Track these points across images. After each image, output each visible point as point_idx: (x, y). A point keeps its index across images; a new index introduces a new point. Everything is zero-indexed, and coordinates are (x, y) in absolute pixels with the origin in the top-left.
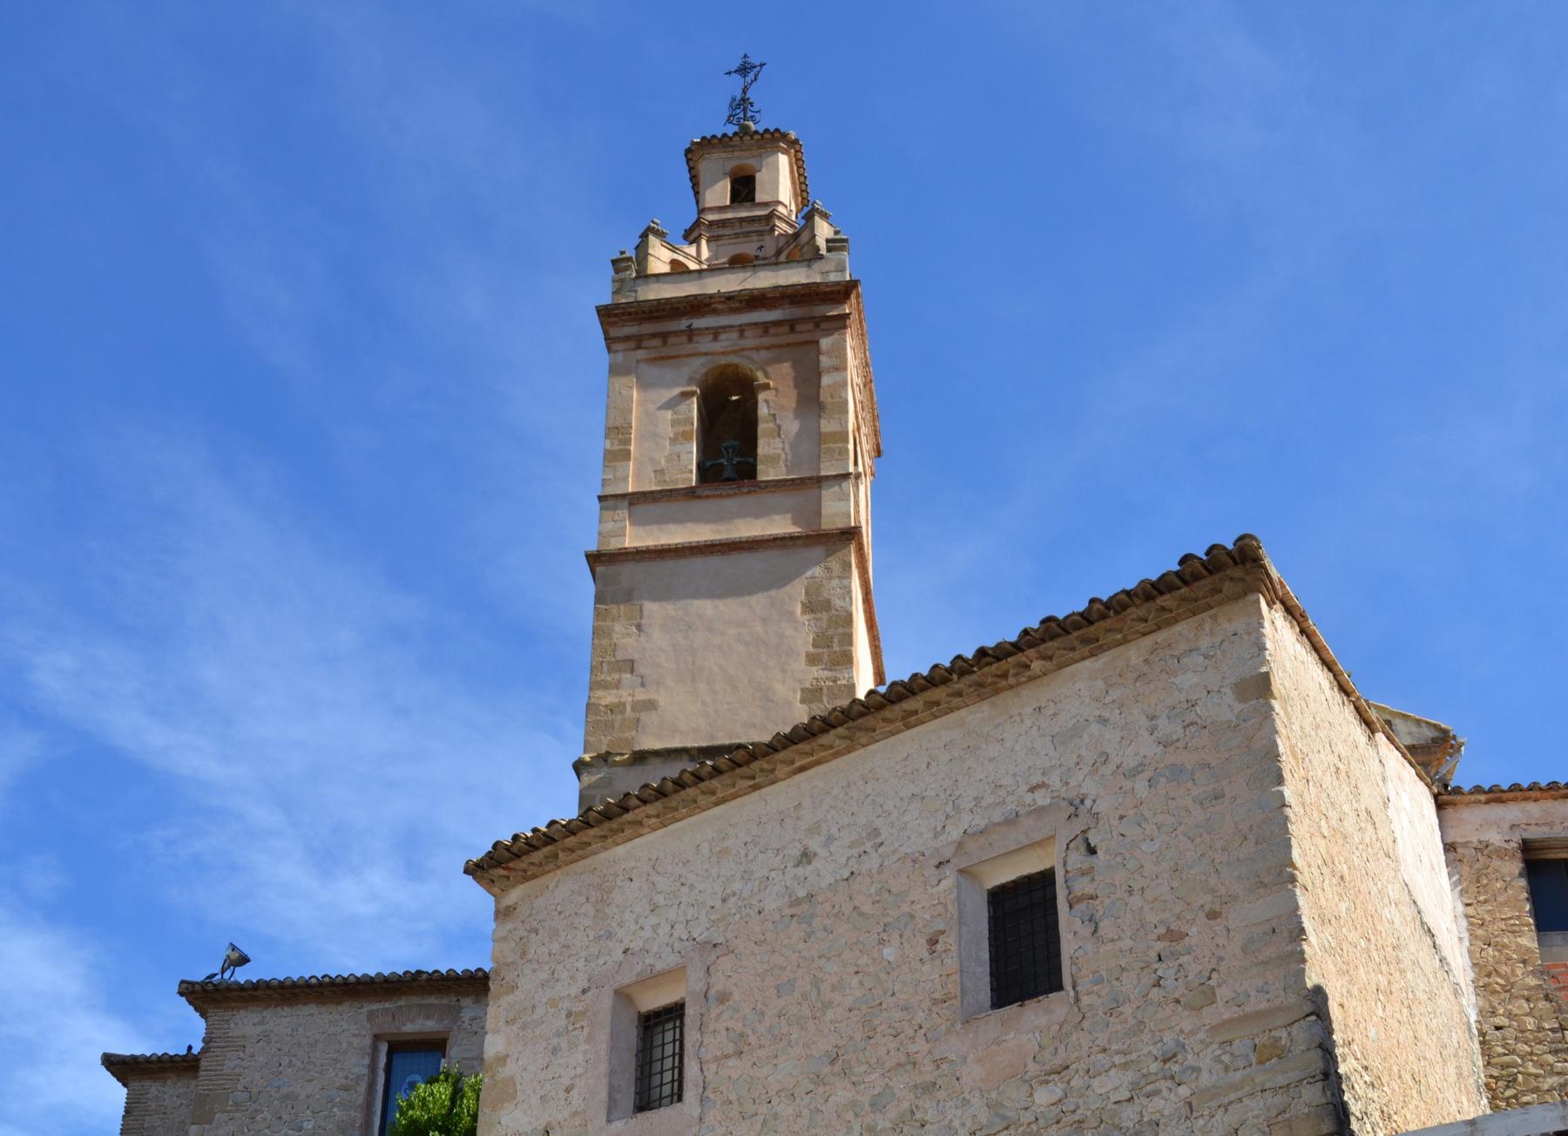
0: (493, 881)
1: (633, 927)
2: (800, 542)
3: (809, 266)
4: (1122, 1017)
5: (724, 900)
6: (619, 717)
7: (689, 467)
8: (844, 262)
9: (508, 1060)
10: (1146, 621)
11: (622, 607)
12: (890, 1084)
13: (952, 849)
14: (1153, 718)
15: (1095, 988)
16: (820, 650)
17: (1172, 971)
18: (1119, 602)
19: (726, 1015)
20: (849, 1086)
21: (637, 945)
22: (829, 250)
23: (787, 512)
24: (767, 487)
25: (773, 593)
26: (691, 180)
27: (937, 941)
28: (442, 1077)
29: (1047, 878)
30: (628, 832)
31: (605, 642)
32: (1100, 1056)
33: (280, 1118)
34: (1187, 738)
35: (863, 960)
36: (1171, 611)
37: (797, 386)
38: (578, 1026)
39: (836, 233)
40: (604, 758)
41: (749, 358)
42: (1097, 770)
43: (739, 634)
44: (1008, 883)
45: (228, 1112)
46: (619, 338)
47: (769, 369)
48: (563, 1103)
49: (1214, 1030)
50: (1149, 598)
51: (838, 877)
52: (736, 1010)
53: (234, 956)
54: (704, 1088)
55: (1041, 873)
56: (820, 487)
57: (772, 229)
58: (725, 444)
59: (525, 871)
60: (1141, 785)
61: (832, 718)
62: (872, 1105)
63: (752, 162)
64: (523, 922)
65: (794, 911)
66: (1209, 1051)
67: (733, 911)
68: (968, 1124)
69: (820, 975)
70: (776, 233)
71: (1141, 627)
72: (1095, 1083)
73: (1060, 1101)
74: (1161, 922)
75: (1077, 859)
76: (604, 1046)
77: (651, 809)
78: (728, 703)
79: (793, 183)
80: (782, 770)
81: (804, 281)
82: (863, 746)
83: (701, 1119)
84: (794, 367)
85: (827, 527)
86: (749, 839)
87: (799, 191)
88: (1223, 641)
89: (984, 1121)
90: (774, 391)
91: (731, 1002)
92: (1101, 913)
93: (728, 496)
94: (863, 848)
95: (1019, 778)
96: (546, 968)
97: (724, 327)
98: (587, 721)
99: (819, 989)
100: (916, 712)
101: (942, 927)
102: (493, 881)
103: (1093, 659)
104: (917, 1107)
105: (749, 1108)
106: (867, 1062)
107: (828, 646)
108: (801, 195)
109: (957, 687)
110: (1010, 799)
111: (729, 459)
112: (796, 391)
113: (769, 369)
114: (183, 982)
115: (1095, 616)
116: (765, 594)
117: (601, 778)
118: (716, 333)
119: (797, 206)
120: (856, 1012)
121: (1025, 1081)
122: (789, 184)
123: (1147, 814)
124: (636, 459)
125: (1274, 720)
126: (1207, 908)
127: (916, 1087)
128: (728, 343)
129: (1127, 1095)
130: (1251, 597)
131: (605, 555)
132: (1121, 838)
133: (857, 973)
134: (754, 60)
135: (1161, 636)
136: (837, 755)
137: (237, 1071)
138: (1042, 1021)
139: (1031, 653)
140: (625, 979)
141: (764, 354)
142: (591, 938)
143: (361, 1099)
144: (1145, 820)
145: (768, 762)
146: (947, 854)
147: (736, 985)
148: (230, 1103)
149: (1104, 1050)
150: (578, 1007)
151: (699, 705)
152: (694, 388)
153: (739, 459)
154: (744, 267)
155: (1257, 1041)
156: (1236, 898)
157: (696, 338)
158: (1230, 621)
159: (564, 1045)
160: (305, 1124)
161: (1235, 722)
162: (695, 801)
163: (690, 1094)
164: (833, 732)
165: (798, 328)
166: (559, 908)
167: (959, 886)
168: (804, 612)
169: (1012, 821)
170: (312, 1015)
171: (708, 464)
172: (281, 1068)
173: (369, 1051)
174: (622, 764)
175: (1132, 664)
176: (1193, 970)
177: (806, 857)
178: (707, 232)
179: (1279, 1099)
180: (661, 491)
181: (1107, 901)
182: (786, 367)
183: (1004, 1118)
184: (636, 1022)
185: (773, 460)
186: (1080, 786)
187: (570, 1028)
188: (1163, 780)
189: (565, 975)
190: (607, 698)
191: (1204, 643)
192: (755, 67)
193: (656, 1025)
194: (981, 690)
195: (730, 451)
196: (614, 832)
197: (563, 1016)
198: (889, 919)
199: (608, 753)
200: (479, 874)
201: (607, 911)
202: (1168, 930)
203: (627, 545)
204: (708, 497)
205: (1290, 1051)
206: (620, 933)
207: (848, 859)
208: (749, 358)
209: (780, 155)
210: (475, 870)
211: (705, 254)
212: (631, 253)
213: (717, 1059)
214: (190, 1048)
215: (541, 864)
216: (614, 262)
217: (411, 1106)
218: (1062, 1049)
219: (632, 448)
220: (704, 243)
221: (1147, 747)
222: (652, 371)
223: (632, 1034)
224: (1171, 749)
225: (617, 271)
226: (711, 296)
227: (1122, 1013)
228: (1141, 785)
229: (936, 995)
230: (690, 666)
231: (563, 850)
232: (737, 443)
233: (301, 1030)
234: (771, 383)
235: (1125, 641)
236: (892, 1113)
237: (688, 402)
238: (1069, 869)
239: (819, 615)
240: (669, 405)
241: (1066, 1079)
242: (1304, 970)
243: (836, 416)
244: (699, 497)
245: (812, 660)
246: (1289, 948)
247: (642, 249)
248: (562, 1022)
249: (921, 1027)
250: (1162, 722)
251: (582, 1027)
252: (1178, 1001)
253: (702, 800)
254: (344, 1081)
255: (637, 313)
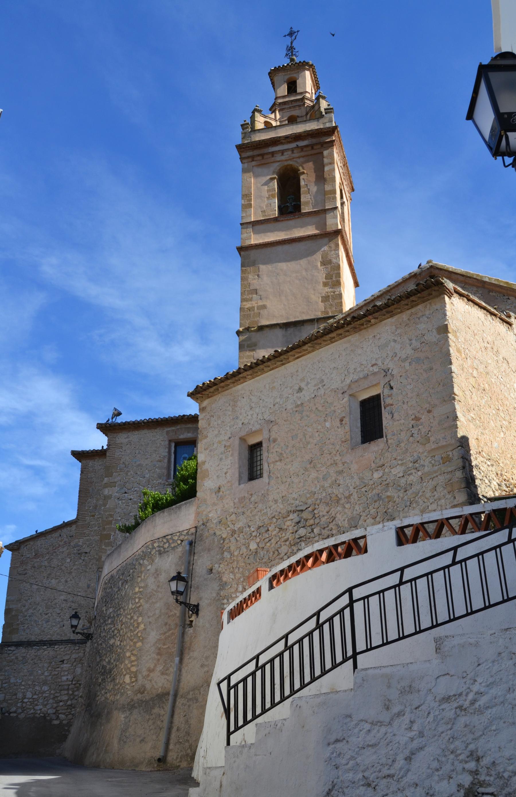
0: (197, 398)
1: (245, 415)
2: (319, 237)
3: (318, 121)
4: (401, 447)
5: (274, 405)
6: (253, 312)
7: (275, 209)
8: (332, 118)
9: (206, 463)
10: (408, 305)
11: (251, 268)
12: (329, 471)
13: (347, 387)
14: (411, 340)
15: (393, 437)
16: (328, 280)
17: (417, 431)
18: (397, 299)
19: (276, 446)
20: (316, 472)
21: (246, 421)
22: (326, 114)
23: (313, 225)
24: (305, 215)
25: (309, 258)
26: (272, 84)
27: (343, 420)
28: (193, 457)
29: (378, 397)
30: (242, 380)
31: (245, 282)
32: (394, 461)
33: (137, 473)
34: (422, 348)
35: (320, 427)
36: (416, 301)
37: (315, 172)
38: (228, 450)
39: (329, 105)
40: (247, 329)
41: (296, 161)
42: (393, 359)
43: (297, 276)
44: (366, 399)
45: (118, 472)
46: (245, 157)
47: (304, 166)
48: (224, 478)
49: (429, 452)
50: (408, 298)
51: (311, 397)
52: (279, 445)
53: (116, 412)
54: (270, 473)
55: (377, 395)
56: (326, 213)
57: (304, 104)
58: (289, 197)
59: (208, 395)
60: (407, 364)
61: (306, 341)
62: (323, 478)
63: (295, 75)
64: (209, 413)
65: (297, 409)
66: (428, 459)
67: (277, 409)
68: (353, 485)
69: (306, 432)
70: (306, 105)
71: (406, 307)
72: (392, 470)
73: (381, 477)
74: (413, 414)
75: (387, 391)
76: (237, 458)
77: (248, 373)
78: (293, 304)
79: (313, 81)
80: (291, 358)
81: (316, 128)
82: (318, 349)
83: (269, 483)
84: (314, 164)
85: (329, 230)
86: (281, 383)
87: (315, 84)
88: (433, 312)
89: (358, 484)
90: (306, 175)
91: (277, 442)
92: (394, 410)
93: (291, 219)
94: (319, 387)
95: (368, 362)
96: (217, 429)
97: (286, 150)
98: (240, 315)
99: (305, 437)
100: (334, 338)
101: (344, 415)
102: (197, 398)
103: (392, 318)
104: (337, 479)
105: (284, 480)
106: (321, 463)
107: (331, 279)
108: (316, 85)
109: (347, 329)
110: (365, 369)
111: (291, 203)
112: (315, 174)
113: (304, 166)
114: (98, 424)
115: (390, 304)
116: (306, 259)
117: (246, 337)
118: (282, 152)
119: (315, 90)
120: (317, 445)
121: (371, 470)
122: (310, 82)
123: (409, 375)
124: (254, 207)
125: (449, 341)
126: (427, 409)
127: (337, 472)
128: (287, 156)
129: (402, 475)
130: (442, 296)
131: (244, 247)
132: (401, 384)
133: (317, 431)
134: (295, 29)
135: (413, 310)
136: (309, 353)
137: (120, 456)
138: (376, 449)
139: (370, 317)
140: (243, 434)
141: (302, 160)
142: (231, 419)
143: (165, 465)
144: (408, 377)
145: (286, 356)
146: (346, 389)
147: (279, 436)
148: (118, 469)
149: (395, 459)
150: (228, 444)
151: (282, 306)
152: (275, 176)
153: (294, 203)
154: (293, 123)
155: (443, 456)
156: (436, 405)
157: (275, 155)
158: (435, 305)
159: (224, 458)
160: (146, 475)
161: (437, 342)
162: (263, 369)
163: (265, 475)
164: (307, 345)
165: (315, 147)
166: (220, 408)
167: (349, 401)
168: (321, 265)
169: (366, 377)
170: (146, 433)
171: (282, 206)
172: (136, 455)
173: (168, 446)
174: (254, 331)
175: (404, 320)
176: (423, 430)
177: (300, 390)
178: (278, 107)
179: (448, 476)
180: (264, 220)
181: (396, 406)
182: (311, 165)
183: (364, 483)
184: (247, 449)
185: (307, 203)
186: (388, 365)
187: (226, 451)
188: (414, 363)
189: (223, 432)
190: (248, 305)
191: (427, 313)
192: (295, 32)
193: (254, 449)
194: (355, 330)
195: (291, 200)
196: (237, 381)
197: (223, 447)
198: (327, 412)
199: (249, 327)
200: (192, 396)
201: (236, 409)
202: (416, 417)
203: (252, 243)
204: (282, 220)
205: (452, 459)
206: (241, 417)
207: (314, 391)
208: (296, 161)
209: (306, 71)
210: (191, 395)
211: (278, 116)
212: (248, 121)
213: (273, 462)
214: (103, 447)
215: (213, 392)
216: (242, 125)
217: (182, 470)
218: (382, 458)
219: (252, 203)
220: (277, 112)
221: (409, 351)
222: (259, 170)
223: (246, 453)
224: (416, 352)
225: (243, 129)
226: (280, 137)
227: (401, 446)
228: (407, 364)
229: (343, 440)
230: (278, 290)
231: (220, 387)
232: (293, 196)
233: (142, 439)
234: (305, 171)
235: (401, 312)
236: (329, 481)
237: (273, 182)
238: (384, 395)
239: (327, 266)
240: (266, 184)
241: (383, 469)
242: (457, 431)
243: (331, 183)
244: (279, 221)
245: (325, 284)
246: (453, 423)
247: (253, 118)
248: (223, 449)
249: (338, 451)
250: (414, 341)
251: (229, 451)
252: (418, 442)
253: (266, 369)
254: (159, 458)
255: (251, 146)
